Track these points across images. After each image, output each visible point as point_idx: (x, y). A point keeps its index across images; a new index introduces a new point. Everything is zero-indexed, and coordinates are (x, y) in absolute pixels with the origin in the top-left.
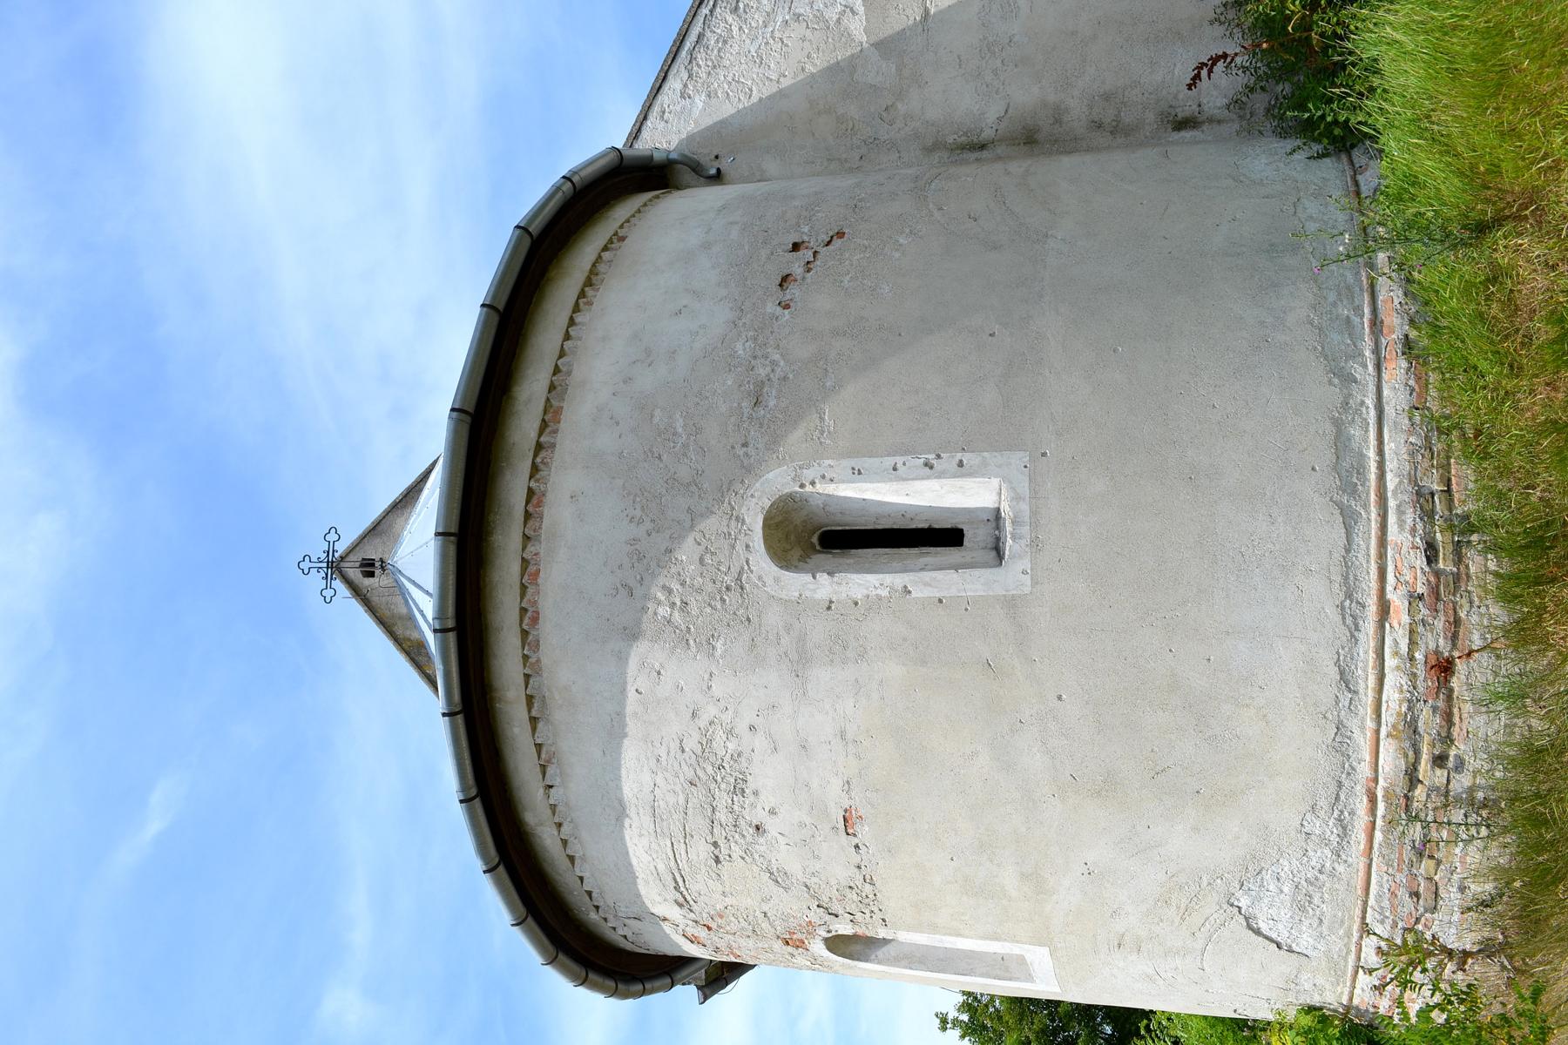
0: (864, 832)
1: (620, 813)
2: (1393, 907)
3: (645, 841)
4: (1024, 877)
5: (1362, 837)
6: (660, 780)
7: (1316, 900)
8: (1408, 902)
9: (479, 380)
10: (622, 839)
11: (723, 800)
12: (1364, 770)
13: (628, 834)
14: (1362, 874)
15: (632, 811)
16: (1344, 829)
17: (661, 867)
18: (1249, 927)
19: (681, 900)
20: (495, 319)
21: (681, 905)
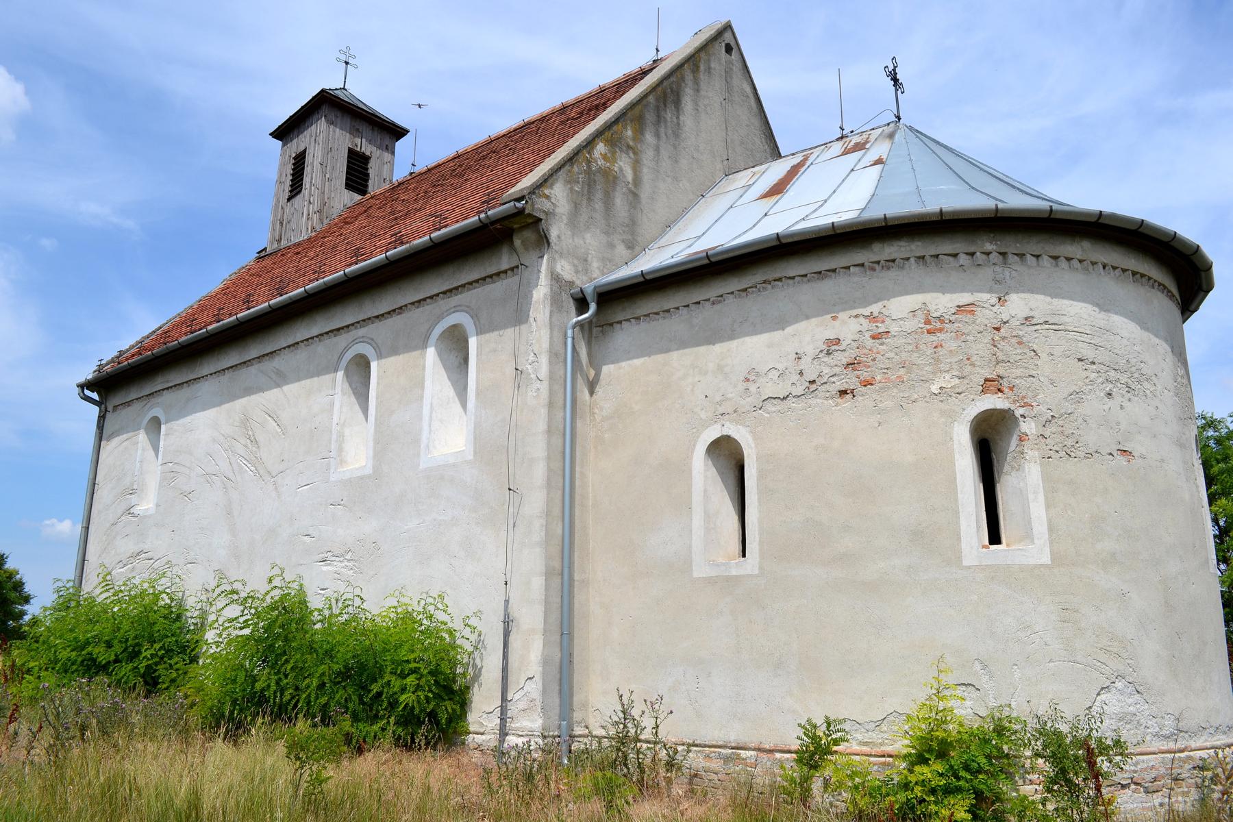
0: (1121, 460)
1: (1102, 307)
2: (1145, 769)
3: (1085, 316)
4: (1113, 555)
5: (1165, 748)
6: (1125, 342)
7: (1128, 726)
8: (1149, 778)
9: (1068, 217)
10: (1089, 302)
11: (1124, 378)
12: (1194, 745)
13: (1090, 307)
14: (1149, 750)
15: (1103, 315)
16: (1167, 737)
17: (1066, 319)
18: (1102, 689)
19: (1034, 321)
20: (1046, 215)
21: (1026, 319)
